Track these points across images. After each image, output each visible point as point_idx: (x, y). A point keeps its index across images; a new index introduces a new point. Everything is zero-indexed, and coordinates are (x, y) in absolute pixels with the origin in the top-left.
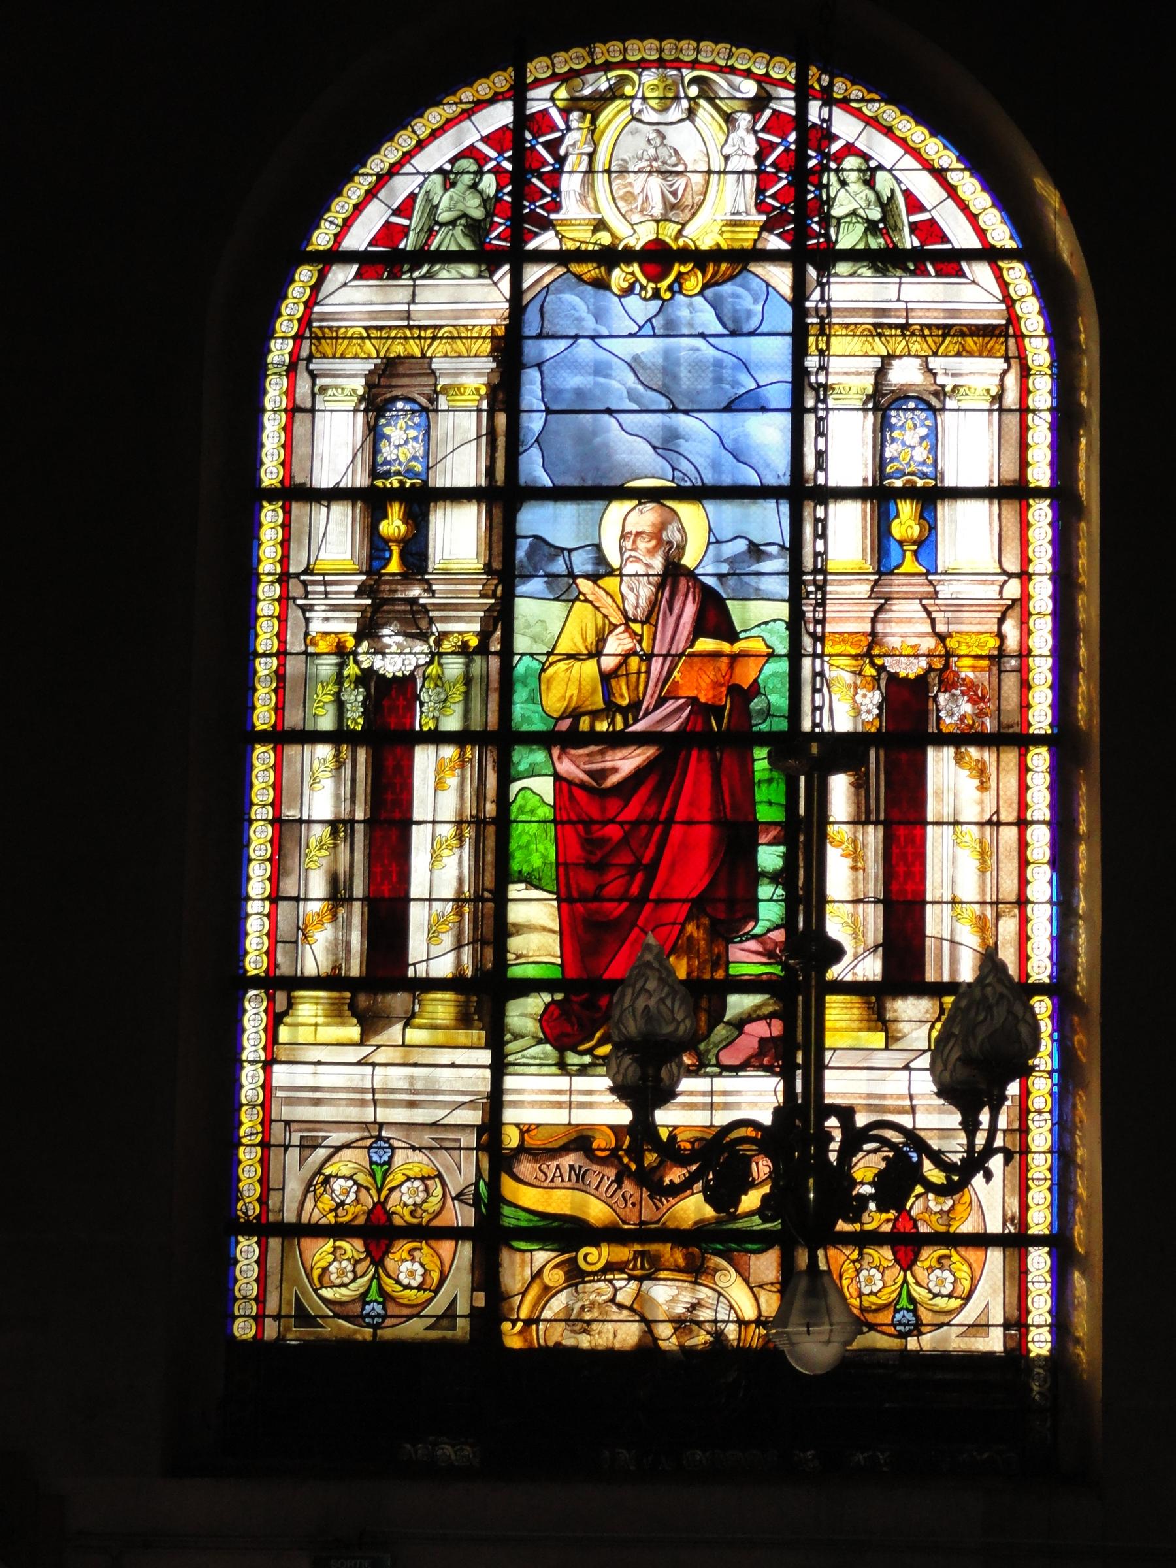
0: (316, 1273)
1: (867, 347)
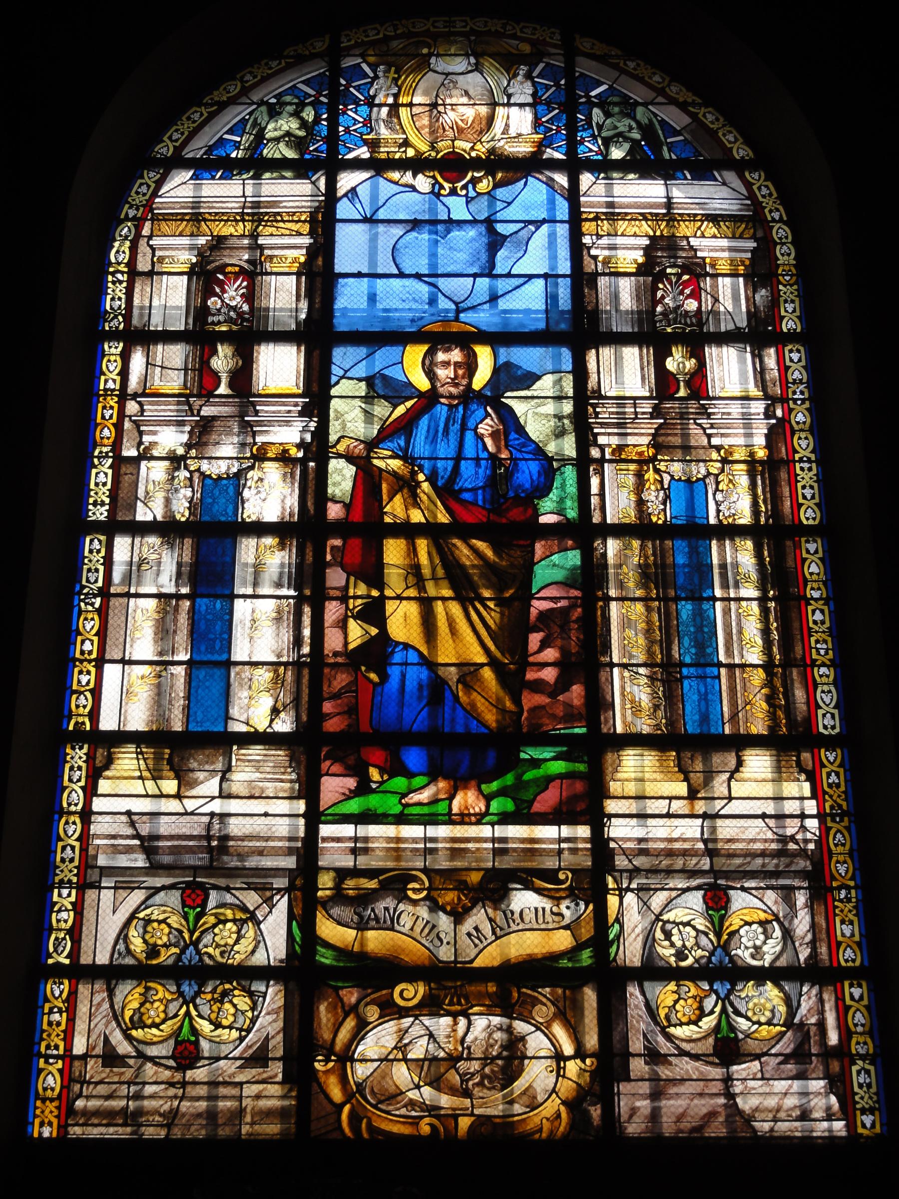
0: (662, 1013)
1: (636, 229)
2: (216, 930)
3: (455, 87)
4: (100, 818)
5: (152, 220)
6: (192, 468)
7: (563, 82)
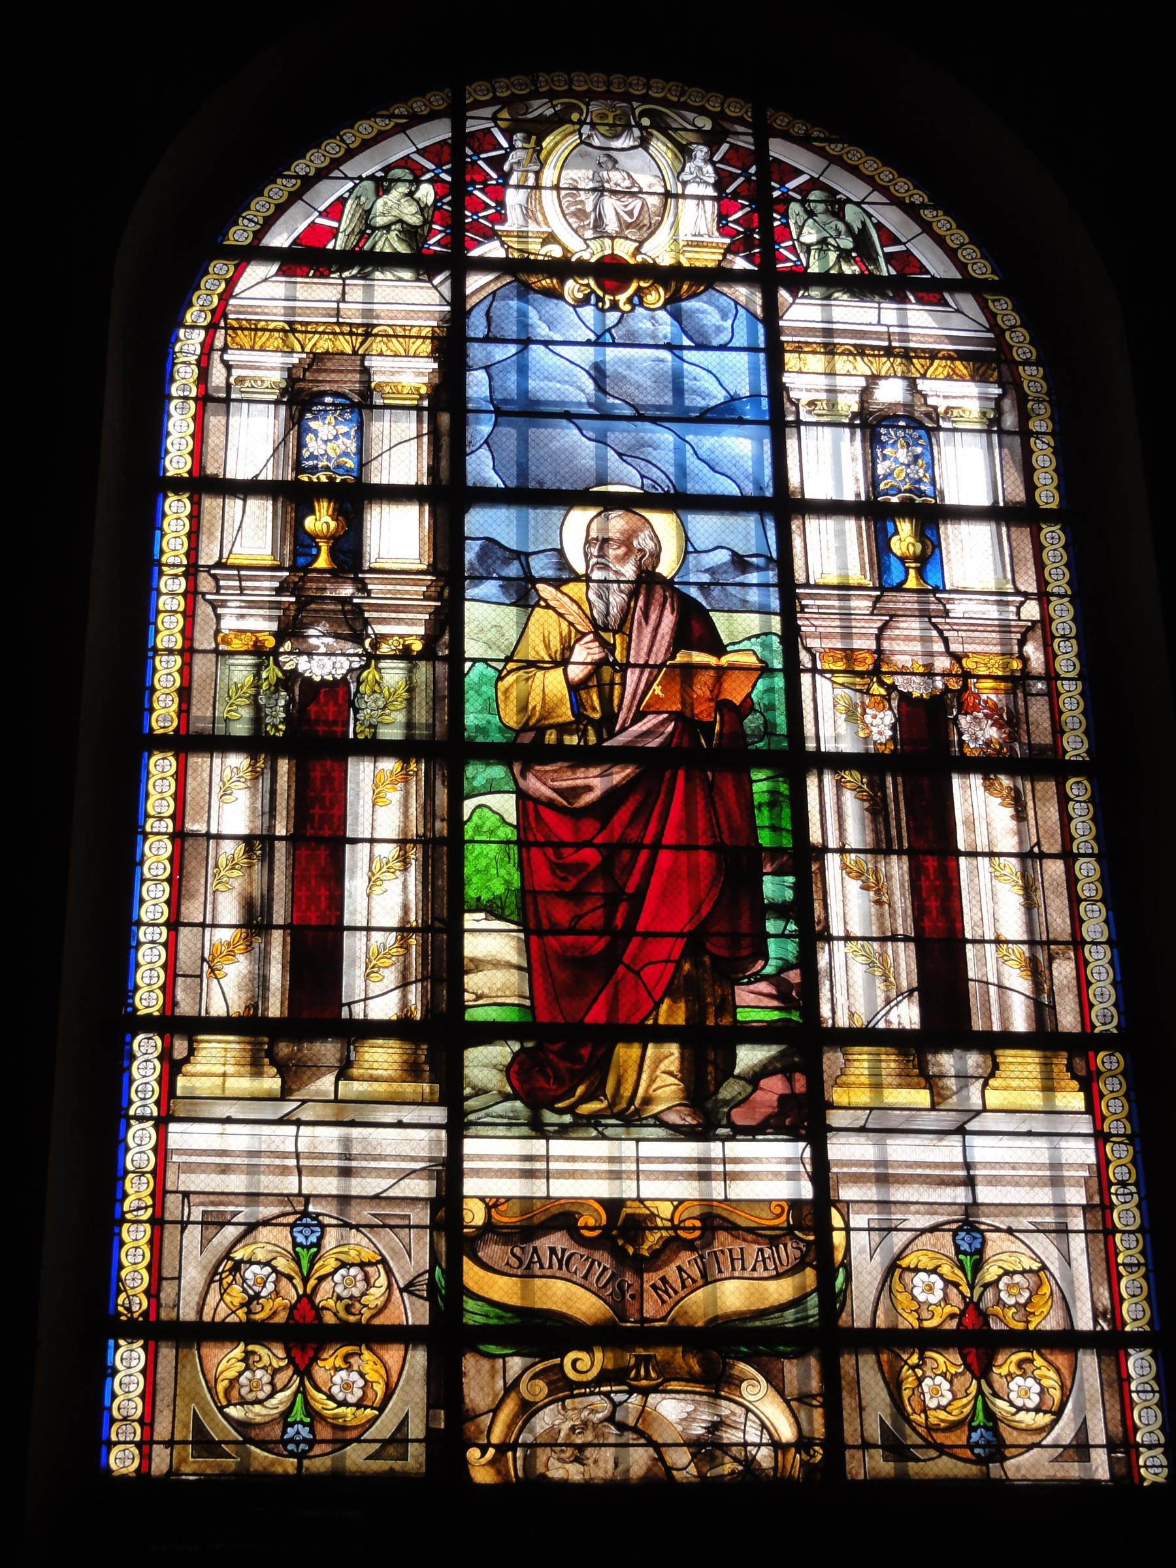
2: (337, 1277)
3: (614, 168)
5: (226, 328)
6: (287, 667)
7: (753, 170)
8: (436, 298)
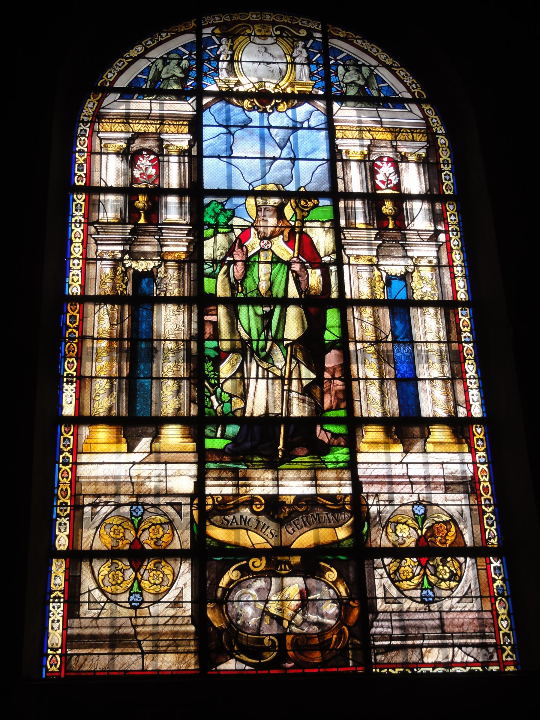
2: (151, 530)
4: (83, 467)
6: (127, 266)
8: (191, 109)
